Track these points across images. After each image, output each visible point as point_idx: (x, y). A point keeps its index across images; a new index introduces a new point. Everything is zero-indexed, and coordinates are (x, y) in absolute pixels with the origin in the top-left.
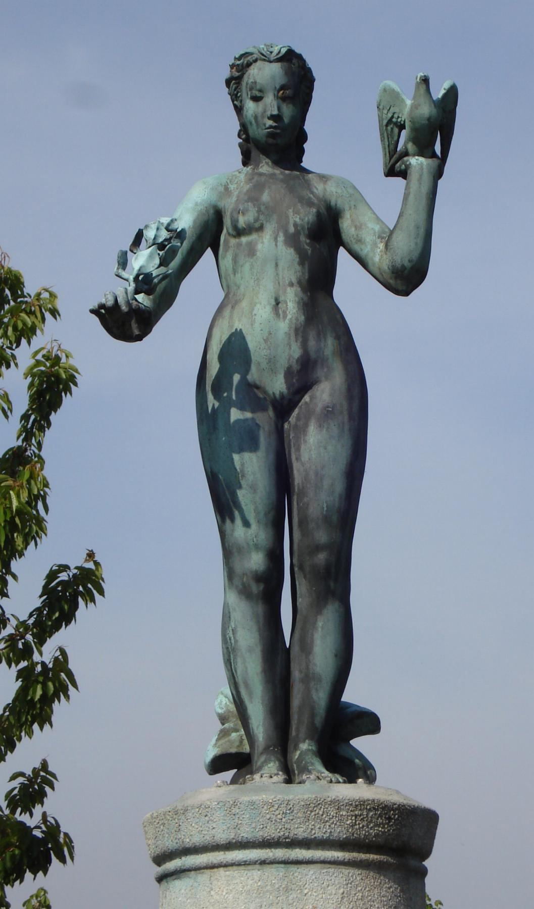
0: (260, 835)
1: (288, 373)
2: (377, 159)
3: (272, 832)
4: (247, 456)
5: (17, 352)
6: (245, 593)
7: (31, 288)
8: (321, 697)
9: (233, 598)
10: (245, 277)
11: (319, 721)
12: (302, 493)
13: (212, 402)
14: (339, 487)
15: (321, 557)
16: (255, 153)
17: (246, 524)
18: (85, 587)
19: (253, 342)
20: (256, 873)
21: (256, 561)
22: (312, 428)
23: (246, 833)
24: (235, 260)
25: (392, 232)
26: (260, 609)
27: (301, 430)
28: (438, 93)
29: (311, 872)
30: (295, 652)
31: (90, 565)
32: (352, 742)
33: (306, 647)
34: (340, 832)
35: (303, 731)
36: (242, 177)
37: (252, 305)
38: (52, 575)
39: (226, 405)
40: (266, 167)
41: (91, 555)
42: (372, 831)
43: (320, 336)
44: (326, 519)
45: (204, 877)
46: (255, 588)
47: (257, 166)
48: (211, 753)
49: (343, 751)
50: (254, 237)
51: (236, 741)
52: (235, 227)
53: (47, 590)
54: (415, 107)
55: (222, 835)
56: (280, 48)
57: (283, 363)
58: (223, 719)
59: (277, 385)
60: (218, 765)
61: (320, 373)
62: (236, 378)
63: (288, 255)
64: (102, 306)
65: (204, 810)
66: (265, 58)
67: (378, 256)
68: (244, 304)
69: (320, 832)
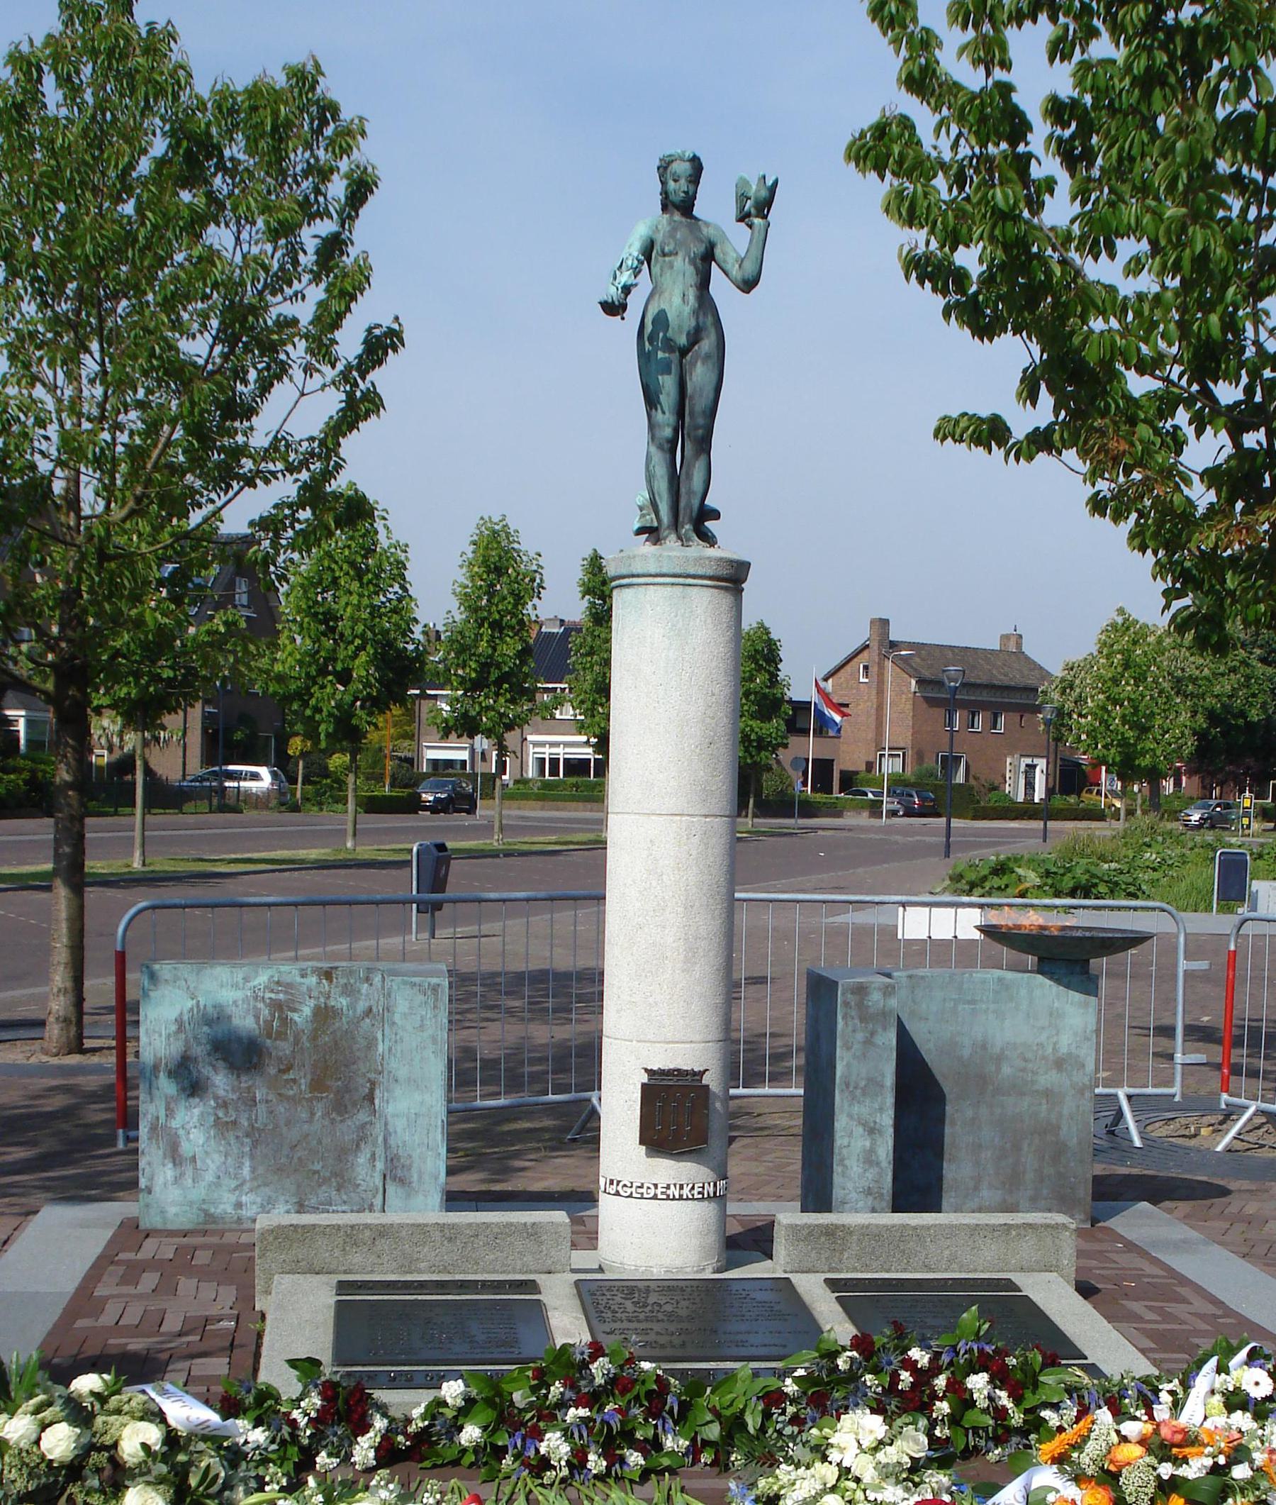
0: (672, 571)
1: (688, 334)
2: (732, 212)
3: (678, 570)
4: (666, 377)
5: (339, 164)
6: (660, 447)
7: (346, 114)
8: (696, 503)
9: (653, 449)
10: (667, 280)
11: (694, 514)
12: (692, 398)
13: (647, 346)
14: (711, 396)
15: (700, 432)
16: (670, 207)
17: (664, 413)
18: (392, 340)
19: (671, 316)
20: (669, 589)
21: (668, 432)
22: (699, 364)
23: (664, 570)
24: (662, 270)
25: (742, 260)
26: (668, 456)
27: (693, 364)
28: (769, 182)
29: (696, 590)
30: (683, 477)
31: (396, 326)
32: (706, 524)
33: (689, 477)
34: (710, 572)
35: (686, 520)
36: (665, 221)
37: (671, 295)
38: (369, 331)
39: (656, 350)
40: (677, 217)
41: (397, 319)
42: (724, 572)
43: (705, 315)
44: (704, 412)
45: (642, 589)
46: (667, 446)
47: (672, 215)
48: (636, 526)
49: (703, 529)
50: (672, 258)
51: (651, 520)
52: (663, 251)
53: (366, 342)
54: (758, 191)
55: (653, 571)
56: (689, 154)
57: (686, 329)
58: (641, 509)
59: (682, 340)
60: (640, 532)
61: (703, 334)
62: (661, 335)
63: (690, 270)
64: (606, 302)
65: (644, 557)
66: (682, 159)
67: (735, 271)
68: (666, 294)
69: (701, 572)
